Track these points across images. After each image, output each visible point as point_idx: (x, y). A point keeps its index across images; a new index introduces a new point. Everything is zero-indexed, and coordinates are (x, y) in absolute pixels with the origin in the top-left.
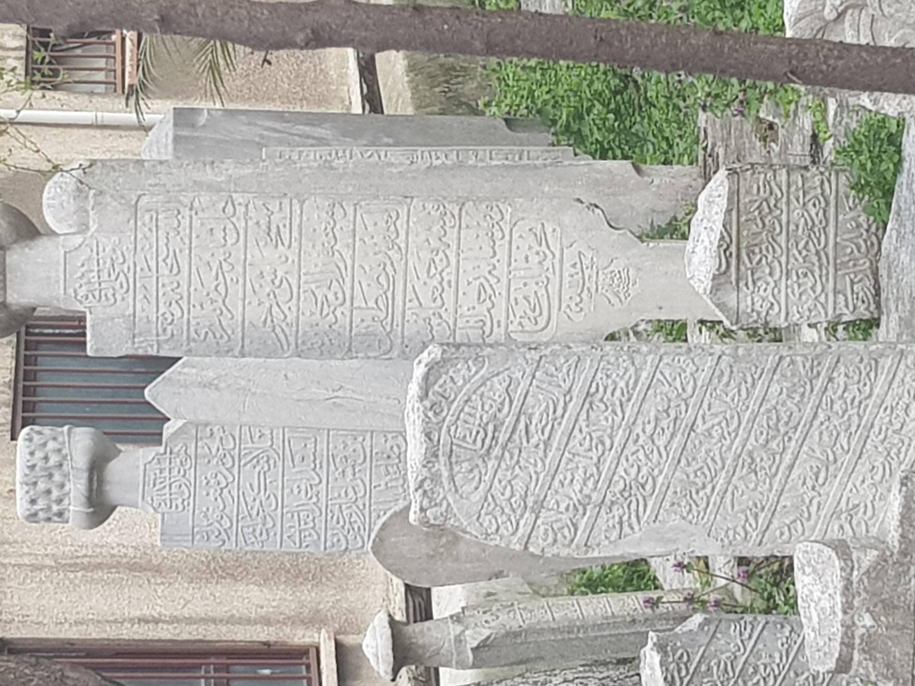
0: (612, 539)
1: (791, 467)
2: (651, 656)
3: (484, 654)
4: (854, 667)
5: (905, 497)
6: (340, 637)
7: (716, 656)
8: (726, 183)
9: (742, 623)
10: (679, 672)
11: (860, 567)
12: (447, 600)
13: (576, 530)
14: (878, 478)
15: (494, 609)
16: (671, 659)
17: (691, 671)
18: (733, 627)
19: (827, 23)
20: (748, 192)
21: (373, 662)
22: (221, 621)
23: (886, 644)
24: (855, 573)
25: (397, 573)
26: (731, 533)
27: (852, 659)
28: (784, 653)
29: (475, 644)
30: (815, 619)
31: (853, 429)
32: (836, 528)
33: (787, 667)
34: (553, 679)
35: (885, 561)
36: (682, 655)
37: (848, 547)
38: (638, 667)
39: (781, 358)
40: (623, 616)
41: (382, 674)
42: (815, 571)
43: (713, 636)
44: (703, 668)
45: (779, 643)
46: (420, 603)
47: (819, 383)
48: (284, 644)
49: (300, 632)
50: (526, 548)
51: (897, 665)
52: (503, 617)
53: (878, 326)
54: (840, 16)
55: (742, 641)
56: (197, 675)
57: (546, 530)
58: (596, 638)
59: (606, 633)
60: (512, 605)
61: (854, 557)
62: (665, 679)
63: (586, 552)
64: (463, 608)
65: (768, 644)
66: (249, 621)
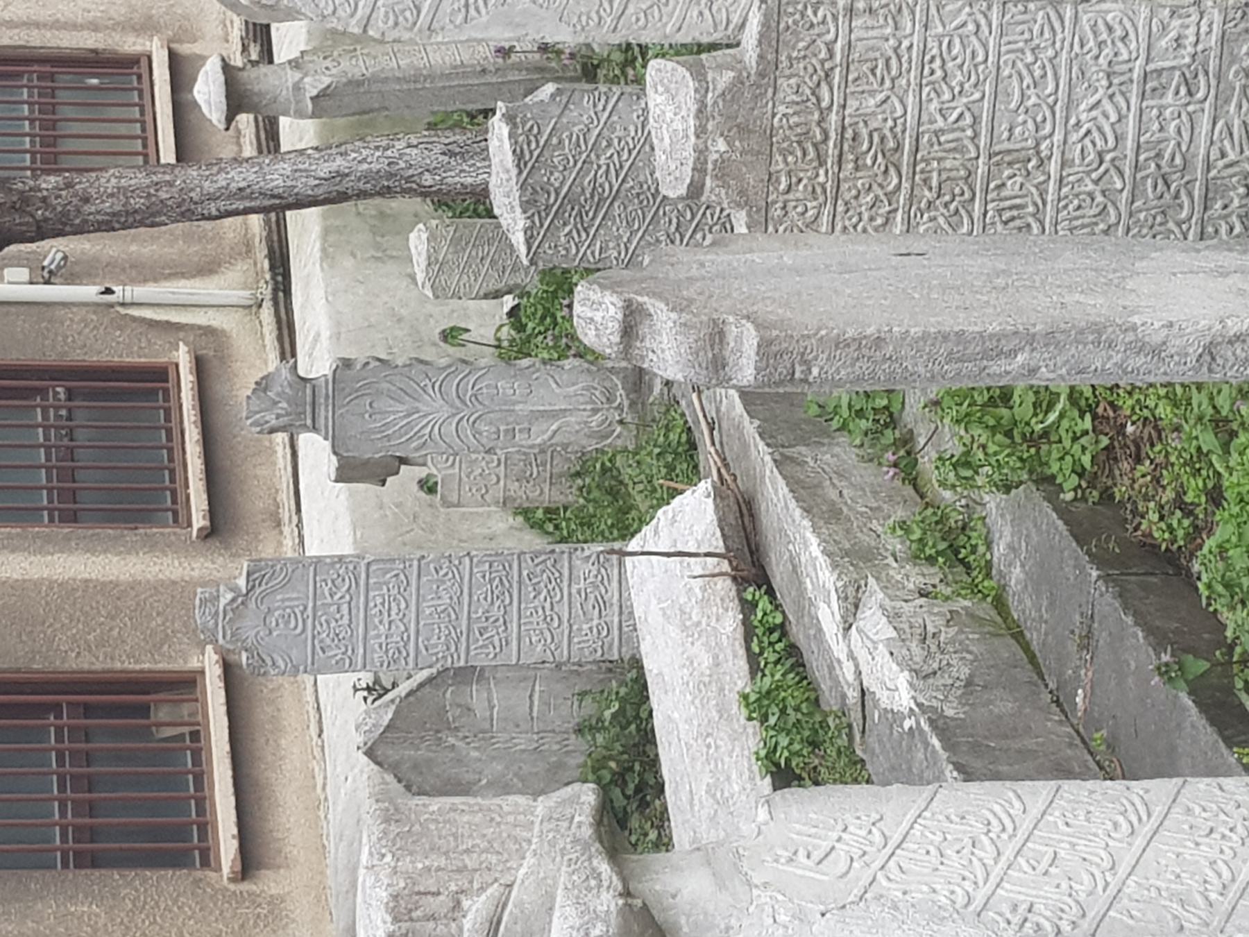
0: (458, 22)
2: (500, 128)
3: (325, 103)
4: (706, 193)
5: (765, 15)
6: (173, 46)
7: (568, 129)
9: (596, 93)
10: (529, 144)
11: (714, 89)
12: (289, 39)
13: (418, 16)
15: (336, 53)
16: (520, 131)
17: (542, 143)
18: (586, 99)
21: (205, 110)
22: (45, 25)
23: (740, 170)
24: (710, 95)
25: (235, 7)
26: (584, 18)
27: (703, 185)
28: (640, 126)
29: (315, 92)
30: (667, 141)
32: (695, 13)
33: (642, 140)
34: (396, 143)
35: (742, 83)
36: (532, 127)
37: (703, 66)
38: (487, 131)
40: (472, 66)
41: (215, 122)
42: (667, 90)
43: (566, 106)
44: (555, 141)
45: (635, 115)
46: (260, 35)
48: (116, 53)
49: (131, 39)
50: (365, 31)
52: (345, 64)
55: (596, 113)
56: (19, 83)
57: (387, 13)
58: (444, 88)
59: (456, 83)
60: (355, 50)
61: (709, 79)
62: (514, 151)
63: (430, 37)
64: (302, 52)
65: (623, 116)
66: (75, 27)
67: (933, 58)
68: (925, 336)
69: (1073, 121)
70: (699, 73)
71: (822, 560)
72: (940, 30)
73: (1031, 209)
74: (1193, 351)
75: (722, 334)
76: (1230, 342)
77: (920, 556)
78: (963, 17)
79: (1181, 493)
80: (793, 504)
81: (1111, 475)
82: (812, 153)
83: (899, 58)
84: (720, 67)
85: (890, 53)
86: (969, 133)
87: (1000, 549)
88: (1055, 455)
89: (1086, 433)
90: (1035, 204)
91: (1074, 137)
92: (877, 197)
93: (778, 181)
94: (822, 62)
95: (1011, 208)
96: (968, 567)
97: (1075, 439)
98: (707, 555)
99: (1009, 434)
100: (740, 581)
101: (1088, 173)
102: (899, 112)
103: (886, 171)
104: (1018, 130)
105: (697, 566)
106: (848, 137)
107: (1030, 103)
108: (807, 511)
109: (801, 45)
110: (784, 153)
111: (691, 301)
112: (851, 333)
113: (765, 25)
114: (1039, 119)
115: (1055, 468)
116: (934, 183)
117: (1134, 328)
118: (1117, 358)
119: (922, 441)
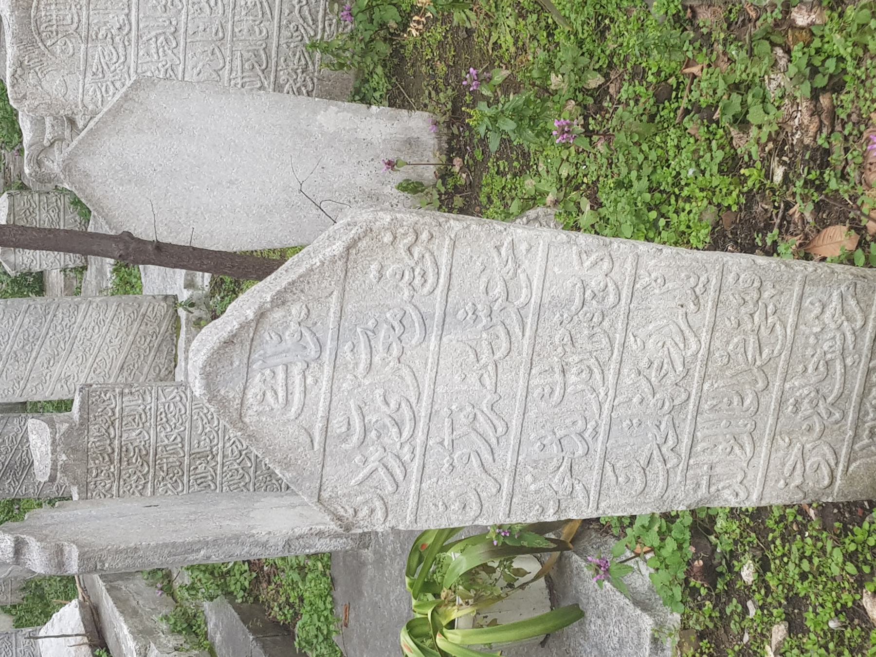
1: (36, 358)
8: (7, 200)
14: (80, 362)
19: (45, 148)
20: (19, 205)
26: (6, 391)
31: (67, 339)
39: (29, 306)
47: (49, 317)
51: (79, 478)
53: (87, 269)
54: (52, 144)
61: (57, 426)
67: (161, 414)
68: (157, 546)
69: (227, 438)
70: (51, 424)
71: (129, 637)
72: (164, 400)
73: (210, 478)
74: (281, 544)
75: (62, 551)
76: (297, 539)
77: (173, 631)
78: (174, 394)
79: (288, 599)
80: (115, 609)
81: (258, 590)
82: (107, 458)
83: (146, 413)
84: (62, 422)
85: (141, 411)
86: (180, 445)
87: (211, 626)
88: (233, 582)
89: (246, 571)
90: (212, 475)
91: (228, 445)
92: (139, 477)
93: (92, 472)
94: (110, 417)
95: (201, 478)
96: (197, 635)
97: (241, 574)
98: (76, 635)
99: (212, 573)
100: (93, 646)
101: (235, 460)
102: (147, 438)
103: (142, 465)
104: (202, 443)
105: (72, 641)
106: (124, 450)
107: (207, 431)
108: (122, 612)
109: (99, 410)
110: (94, 459)
111: (47, 536)
112: (122, 547)
113: (82, 402)
114: (211, 437)
115: (233, 588)
116: (165, 469)
117: (253, 536)
118: (246, 549)
119: (175, 575)
